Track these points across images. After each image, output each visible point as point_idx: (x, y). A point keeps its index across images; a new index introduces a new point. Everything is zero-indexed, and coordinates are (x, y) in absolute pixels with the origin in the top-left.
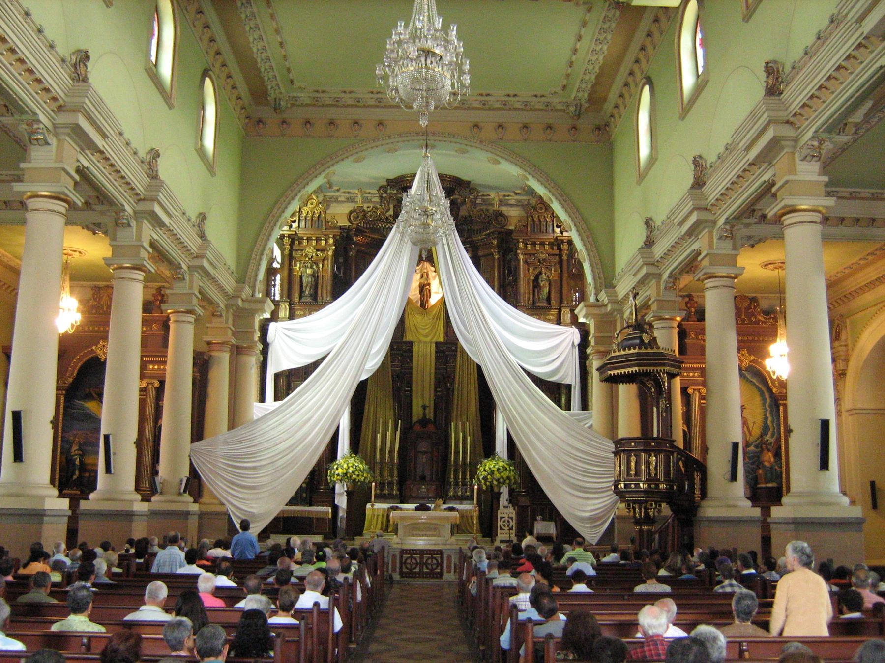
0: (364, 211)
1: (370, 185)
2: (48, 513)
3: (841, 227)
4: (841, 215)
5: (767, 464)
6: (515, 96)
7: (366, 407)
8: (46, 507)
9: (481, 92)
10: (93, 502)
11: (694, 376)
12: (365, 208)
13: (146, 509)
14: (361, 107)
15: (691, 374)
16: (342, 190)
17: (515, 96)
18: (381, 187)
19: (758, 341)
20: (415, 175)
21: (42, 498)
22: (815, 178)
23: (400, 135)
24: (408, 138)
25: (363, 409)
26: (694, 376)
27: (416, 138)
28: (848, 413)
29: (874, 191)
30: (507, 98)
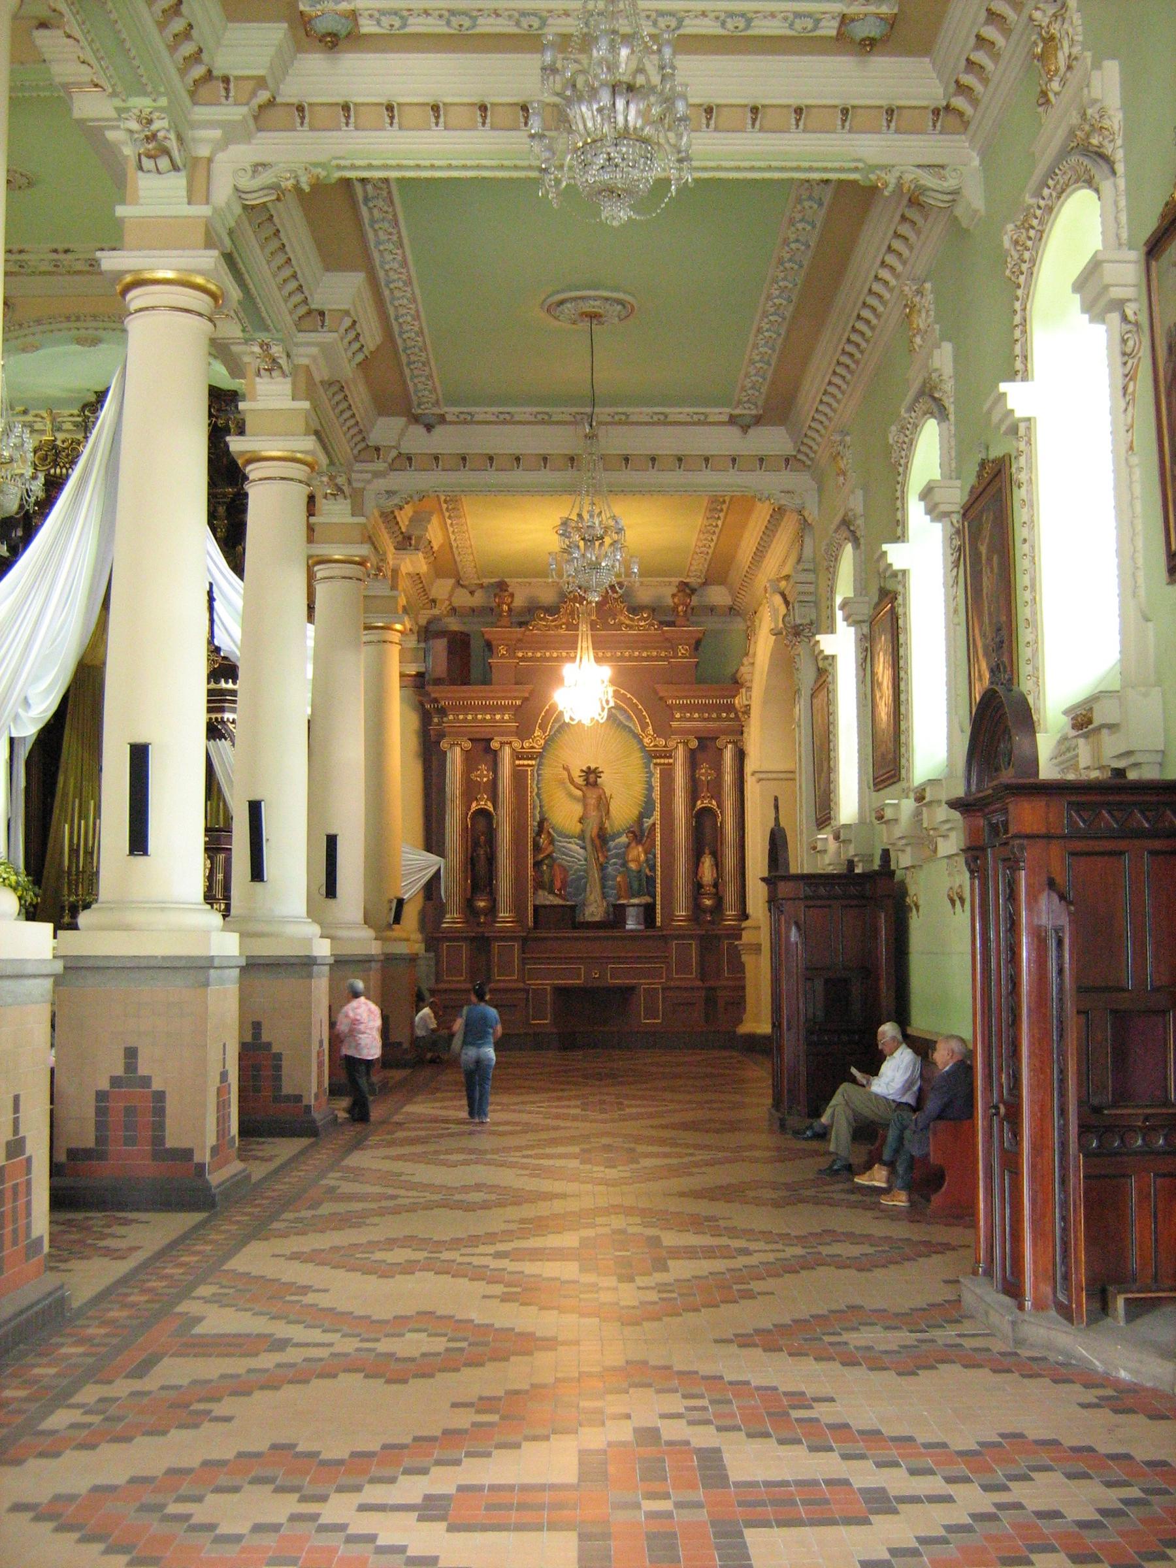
0: (55, 447)
1: (68, 402)
2: (319, 961)
3: (543, 472)
4: (625, 452)
5: (633, 866)
6: (66, 251)
7: (61, 779)
8: (315, 954)
9: (55, 246)
10: (94, 937)
11: (465, 720)
12: (59, 443)
13: (379, 952)
14: (28, 275)
15: (470, 717)
16: (33, 412)
17: (66, 251)
18: (85, 406)
19: (550, 659)
20: (107, 390)
21: (309, 941)
22: (290, 404)
23: (39, 322)
24: (53, 327)
25: (54, 783)
26: (502, 720)
27: (65, 325)
28: (754, 779)
29: (575, 410)
30: (55, 256)
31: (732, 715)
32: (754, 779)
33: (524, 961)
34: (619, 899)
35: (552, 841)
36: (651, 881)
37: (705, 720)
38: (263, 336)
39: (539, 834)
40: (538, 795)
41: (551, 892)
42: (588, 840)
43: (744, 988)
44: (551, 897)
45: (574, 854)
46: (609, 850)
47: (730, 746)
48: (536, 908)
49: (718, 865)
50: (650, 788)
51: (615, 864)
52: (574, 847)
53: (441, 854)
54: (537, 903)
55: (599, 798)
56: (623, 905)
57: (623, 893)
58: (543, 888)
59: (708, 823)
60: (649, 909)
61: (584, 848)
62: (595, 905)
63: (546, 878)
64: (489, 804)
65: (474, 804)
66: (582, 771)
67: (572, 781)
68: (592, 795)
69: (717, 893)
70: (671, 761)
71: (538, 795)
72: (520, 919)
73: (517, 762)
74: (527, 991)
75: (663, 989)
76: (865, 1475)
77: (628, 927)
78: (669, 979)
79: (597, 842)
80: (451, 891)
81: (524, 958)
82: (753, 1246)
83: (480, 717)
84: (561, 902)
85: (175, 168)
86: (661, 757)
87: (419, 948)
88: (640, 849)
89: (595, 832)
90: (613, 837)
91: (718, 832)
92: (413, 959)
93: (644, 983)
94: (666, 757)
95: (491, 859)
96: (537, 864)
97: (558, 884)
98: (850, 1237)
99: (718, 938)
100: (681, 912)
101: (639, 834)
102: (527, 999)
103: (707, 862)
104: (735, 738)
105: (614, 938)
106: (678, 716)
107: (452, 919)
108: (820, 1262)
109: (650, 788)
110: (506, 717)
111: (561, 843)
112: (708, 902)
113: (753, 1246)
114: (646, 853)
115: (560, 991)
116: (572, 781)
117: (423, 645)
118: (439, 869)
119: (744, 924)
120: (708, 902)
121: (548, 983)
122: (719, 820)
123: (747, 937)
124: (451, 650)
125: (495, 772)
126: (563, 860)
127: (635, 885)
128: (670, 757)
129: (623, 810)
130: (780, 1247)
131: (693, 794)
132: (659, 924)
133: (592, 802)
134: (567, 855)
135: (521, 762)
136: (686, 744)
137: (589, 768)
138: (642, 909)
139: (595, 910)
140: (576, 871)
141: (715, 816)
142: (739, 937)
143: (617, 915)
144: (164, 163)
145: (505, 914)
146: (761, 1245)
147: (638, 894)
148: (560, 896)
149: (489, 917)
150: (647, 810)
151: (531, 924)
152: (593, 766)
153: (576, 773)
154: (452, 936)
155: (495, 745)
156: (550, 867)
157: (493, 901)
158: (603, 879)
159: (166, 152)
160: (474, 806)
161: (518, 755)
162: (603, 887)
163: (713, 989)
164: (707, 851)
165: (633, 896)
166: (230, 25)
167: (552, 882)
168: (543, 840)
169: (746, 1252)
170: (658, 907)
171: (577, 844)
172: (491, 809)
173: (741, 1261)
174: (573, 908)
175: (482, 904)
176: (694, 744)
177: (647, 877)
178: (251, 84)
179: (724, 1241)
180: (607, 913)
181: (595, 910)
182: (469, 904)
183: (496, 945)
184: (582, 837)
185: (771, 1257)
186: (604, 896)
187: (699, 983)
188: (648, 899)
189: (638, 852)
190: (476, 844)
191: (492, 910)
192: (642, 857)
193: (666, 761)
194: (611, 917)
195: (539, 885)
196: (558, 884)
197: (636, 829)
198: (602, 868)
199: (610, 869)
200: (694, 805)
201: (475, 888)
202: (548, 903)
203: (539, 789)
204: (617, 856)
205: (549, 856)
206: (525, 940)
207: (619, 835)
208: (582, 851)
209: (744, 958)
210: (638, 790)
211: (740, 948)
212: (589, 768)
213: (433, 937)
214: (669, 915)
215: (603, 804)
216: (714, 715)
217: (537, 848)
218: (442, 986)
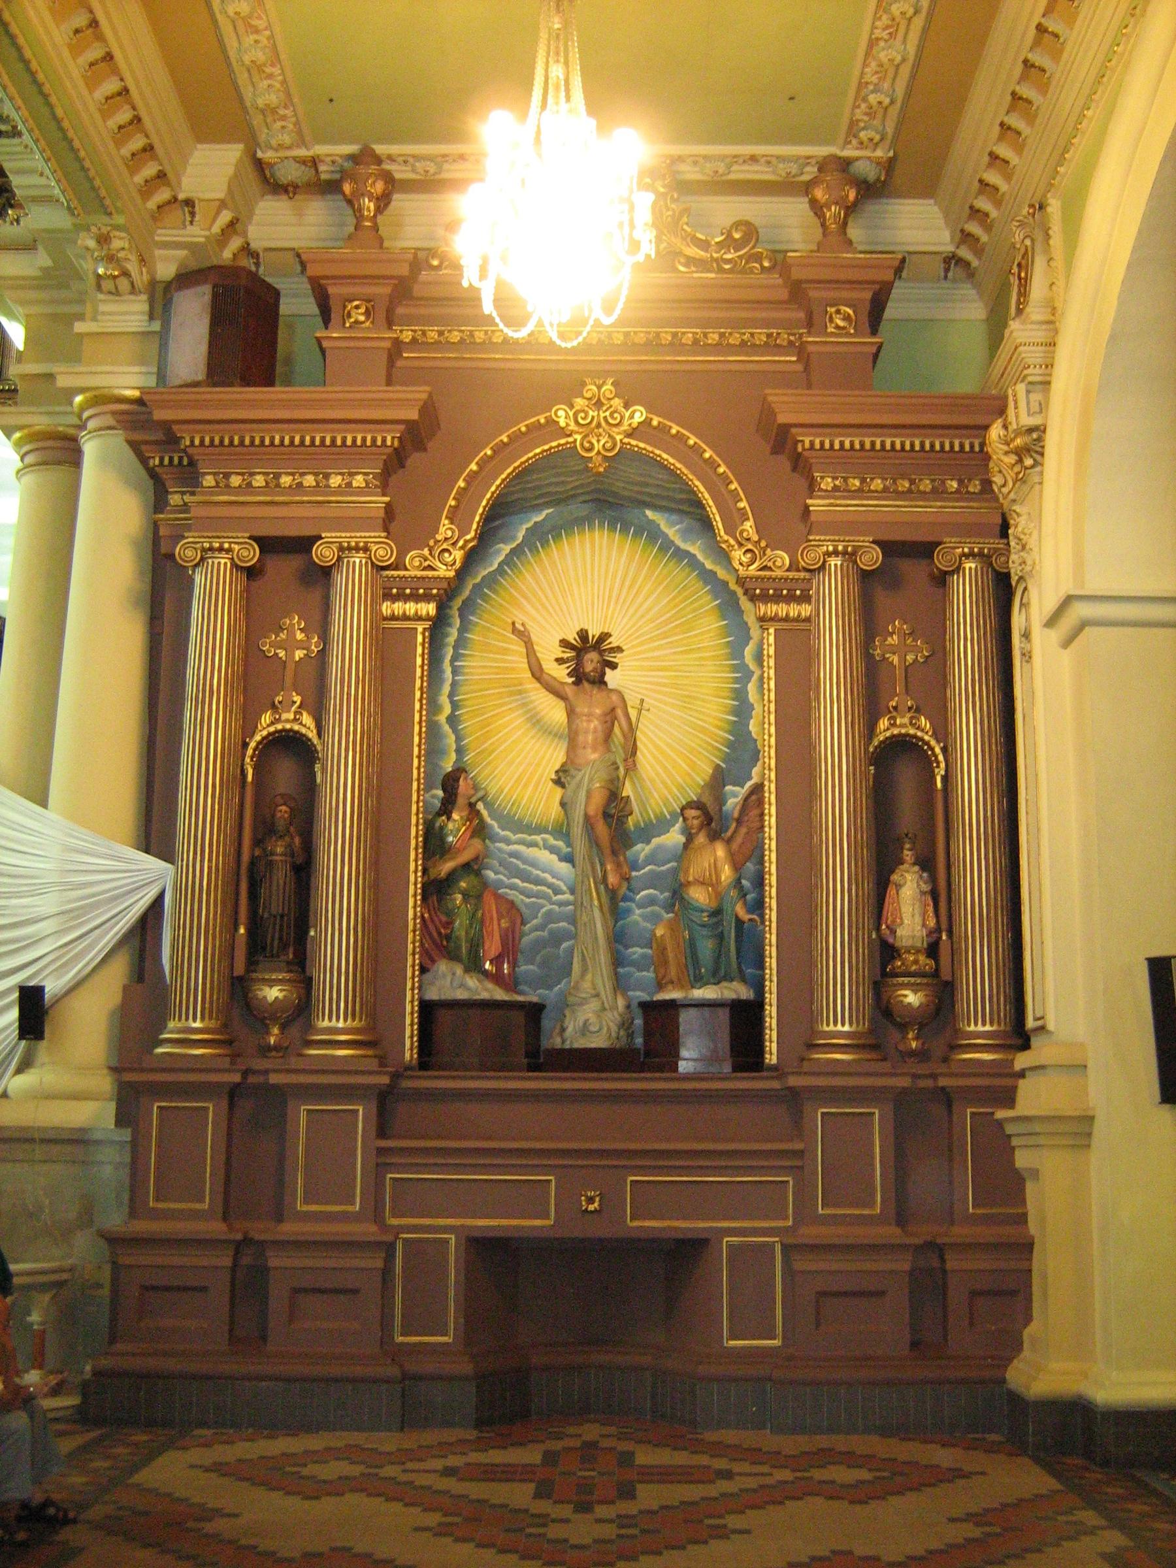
5: (699, 896)
28: (1055, 636)
31: (975, 487)
32: (1055, 636)
33: (381, 1161)
34: (660, 986)
35: (480, 830)
36: (749, 946)
37: (900, 495)
38: (101, 222)
39: (447, 806)
40: (453, 720)
41: (474, 965)
42: (577, 830)
43: (1027, 1247)
44: (472, 982)
45: (542, 871)
46: (634, 866)
47: (969, 565)
48: (427, 1009)
49: (941, 897)
50: (742, 710)
51: (652, 901)
52: (545, 858)
53: (167, 855)
54: (432, 995)
55: (610, 717)
56: (672, 1005)
57: (673, 972)
58: (454, 956)
59: (906, 776)
60: (746, 1017)
61: (569, 859)
62: (594, 1005)
63: (460, 925)
64: (307, 719)
65: (266, 718)
66: (565, 643)
67: (537, 673)
68: (592, 706)
69: (936, 973)
70: (805, 610)
71: (453, 720)
72: (374, 1039)
73: (386, 608)
74: (390, 1248)
75: (785, 1247)
76: (721, 1464)
77: (683, 1067)
78: (804, 1213)
79: (602, 829)
80: (191, 958)
81: (381, 1151)
82: (737, 1467)
83: (286, 480)
84: (500, 995)
85: (133, 290)
86: (778, 598)
87: (95, 1113)
88: (720, 851)
89: (598, 799)
90: (648, 832)
91: (938, 805)
92: (77, 1141)
93: (731, 1232)
94: (791, 598)
95: (304, 869)
96: (436, 890)
97: (493, 946)
98: (850, 1459)
99: (946, 1098)
100: (840, 1026)
101: (707, 817)
102: (387, 1272)
103: (909, 887)
104: (989, 544)
105: (655, 1097)
106: (827, 483)
107: (189, 1028)
108: (802, 1491)
109: (742, 710)
110: (359, 481)
111: (508, 843)
112: (912, 998)
113: (737, 1467)
114: (737, 867)
115: (488, 1251)
116: (537, 673)
117: (156, 326)
118: (161, 897)
119: (1022, 1060)
120: (912, 998)
121: (449, 1229)
122: (940, 772)
123: (1035, 1097)
124: (220, 318)
125: (325, 637)
126: (515, 890)
127: (706, 947)
128: (805, 598)
129: (671, 762)
130: (765, 1469)
131: (870, 700)
132: (772, 1055)
133: (591, 727)
134: (526, 878)
135: (398, 607)
136: (850, 556)
137: (583, 635)
138: (724, 1015)
139: (592, 1016)
140: (550, 917)
141: (925, 761)
142: (1008, 1098)
143: (660, 1019)
144: (124, 283)
145: (335, 1021)
146: (746, 1467)
147: (718, 976)
148: (497, 978)
149: (294, 1031)
150: (739, 751)
151: (409, 1051)
152: (594, 632)
153: (549, 652)
154: (177, 1085)
155: (323, 553)
156: (475, 897)
157: (305, 984)
158: (618, 939)
159: (126, 274)
160: (266, 725)
161: (388, 584)
162: (617, 961)
163: (938, 1249)
164: (908, 855)
165: (699, 980)
166: (199, 146)
167: (475, 945)
168: (455, 826)
169: (728, 1475)
170: (771, 1012)
171: (553, 850)
172: (312, 734)
173: (724, 1486)
174: (535, 1012)
175: (273, 993)
176: (872, 558)
177: (739, 922)
178: (217, 203)
179: (704, 1460)
180: (626, 1024)
181: (592, 1016)
182: (237, 990)
183: (302, 1113)
184: (562, 831)
185: (752, 1483)
186: (620, 984)
187: (216, 1228)
188: (738, 991)
189: (715, 860)
190: (265, 830)
191: (302, 1009)
192: (726, 873)
193: (794, 610)
194: (639, 1041)
195: (440, 945)
196: (493, 946)
197: (707, 800)
198: (615, 905)
199: (637, 915)
200: (871, 729)
201: (257, 948)
202: (461, 995)
203: (455, 706)
204: (653, 881)
205: (472, 868)
206: (385, 1101)
207: (662, 825)
208: (564, 868)
209: (1022, 1160)
210: (714, 711)
211: (1009, 1129)
212: (583, 635)
213: (138, 1083)
214: (805, 1038)
215: (618, 731)
216: (926, 485)
217: (434, 844)
218: (142, 1227)
